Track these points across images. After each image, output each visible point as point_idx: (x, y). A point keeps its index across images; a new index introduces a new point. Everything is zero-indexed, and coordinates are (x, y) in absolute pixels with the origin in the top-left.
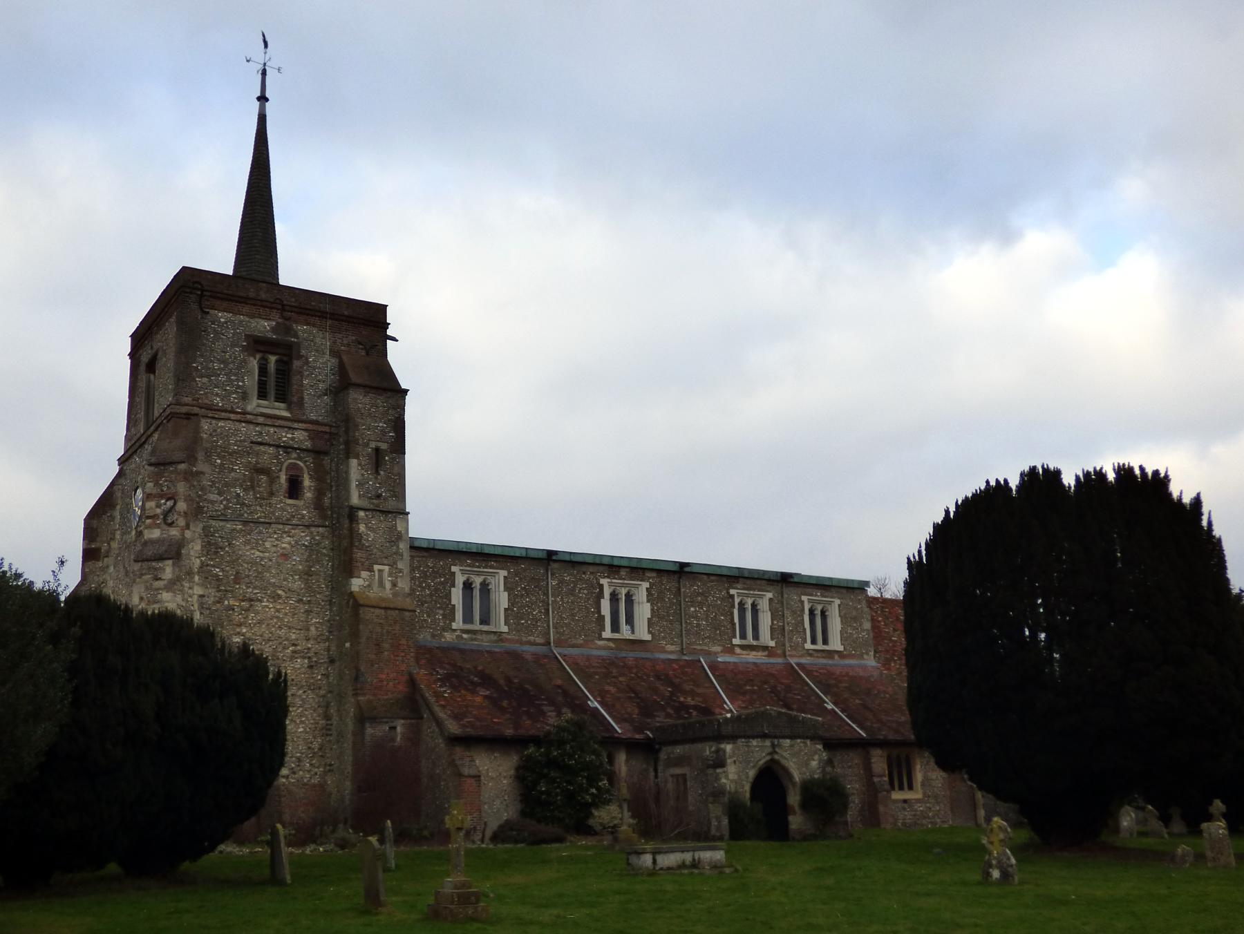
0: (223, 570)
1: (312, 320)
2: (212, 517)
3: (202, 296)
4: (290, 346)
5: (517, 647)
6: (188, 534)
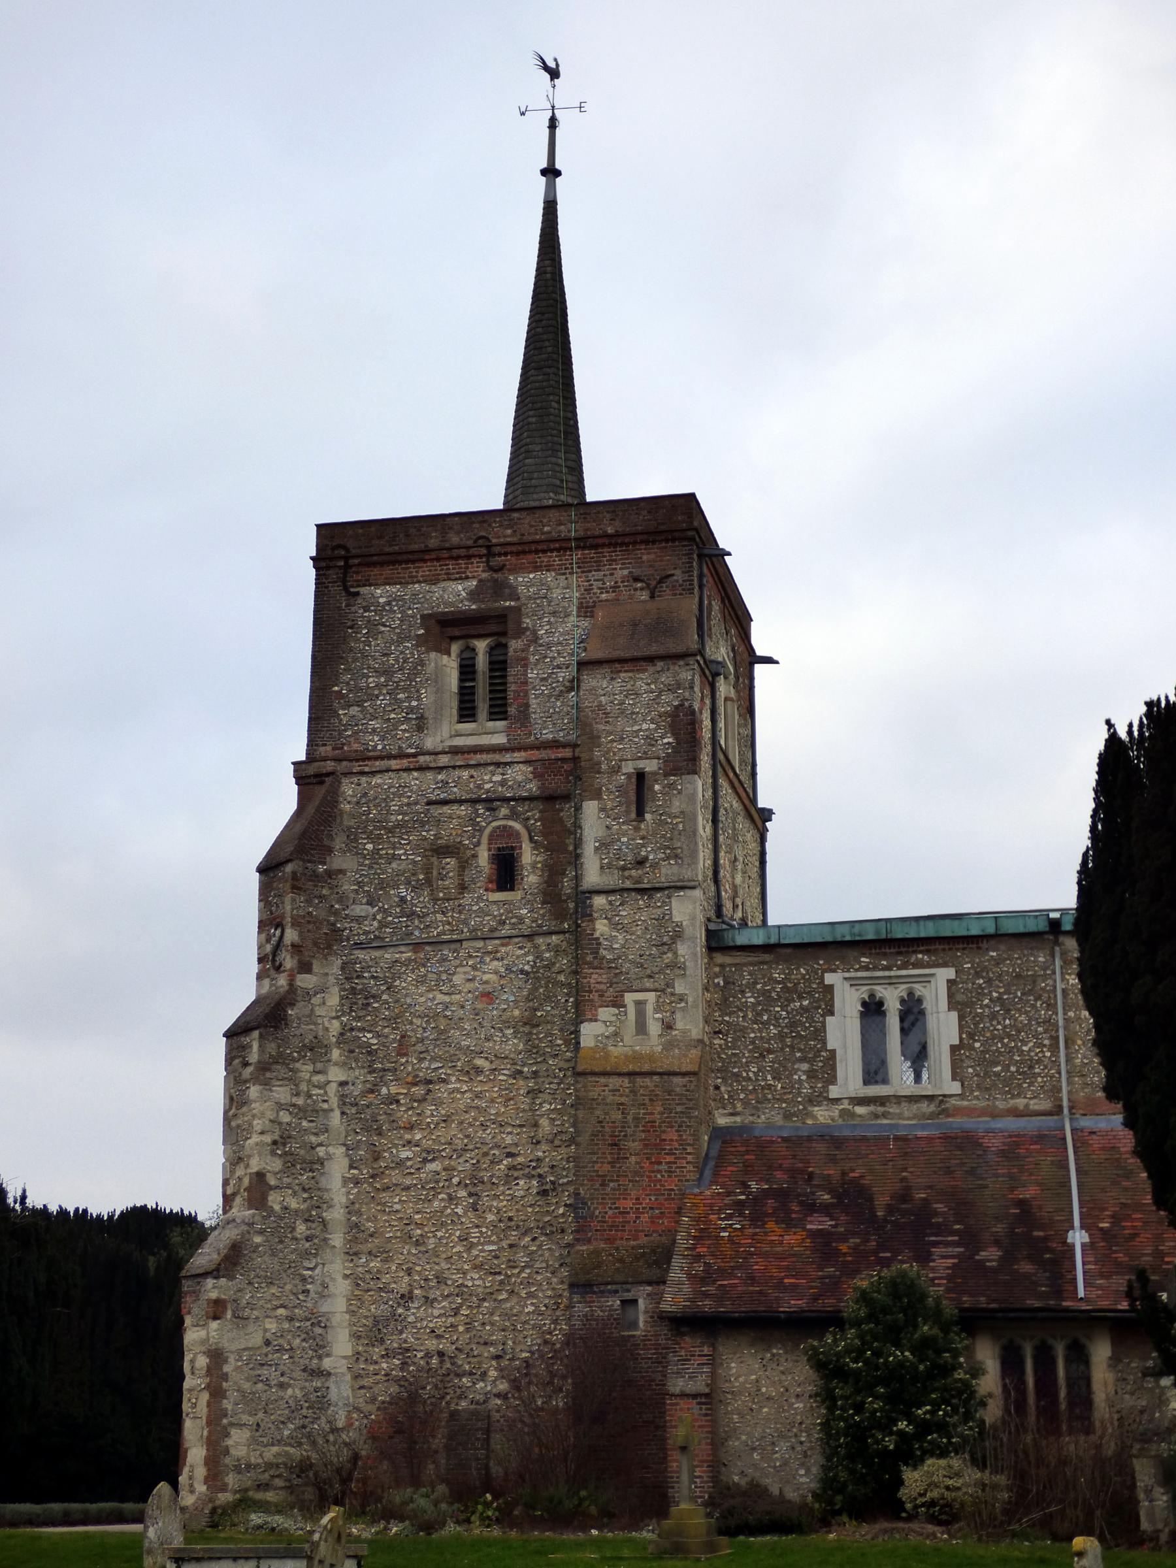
0: (378, 1035)
1: (544, 559)
2: (359, 946)
3: (347, 567)
4: (502, 617)
5: (979, 1124)
6: (305, 981)
